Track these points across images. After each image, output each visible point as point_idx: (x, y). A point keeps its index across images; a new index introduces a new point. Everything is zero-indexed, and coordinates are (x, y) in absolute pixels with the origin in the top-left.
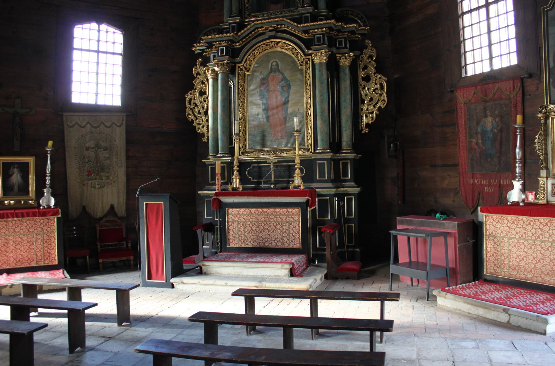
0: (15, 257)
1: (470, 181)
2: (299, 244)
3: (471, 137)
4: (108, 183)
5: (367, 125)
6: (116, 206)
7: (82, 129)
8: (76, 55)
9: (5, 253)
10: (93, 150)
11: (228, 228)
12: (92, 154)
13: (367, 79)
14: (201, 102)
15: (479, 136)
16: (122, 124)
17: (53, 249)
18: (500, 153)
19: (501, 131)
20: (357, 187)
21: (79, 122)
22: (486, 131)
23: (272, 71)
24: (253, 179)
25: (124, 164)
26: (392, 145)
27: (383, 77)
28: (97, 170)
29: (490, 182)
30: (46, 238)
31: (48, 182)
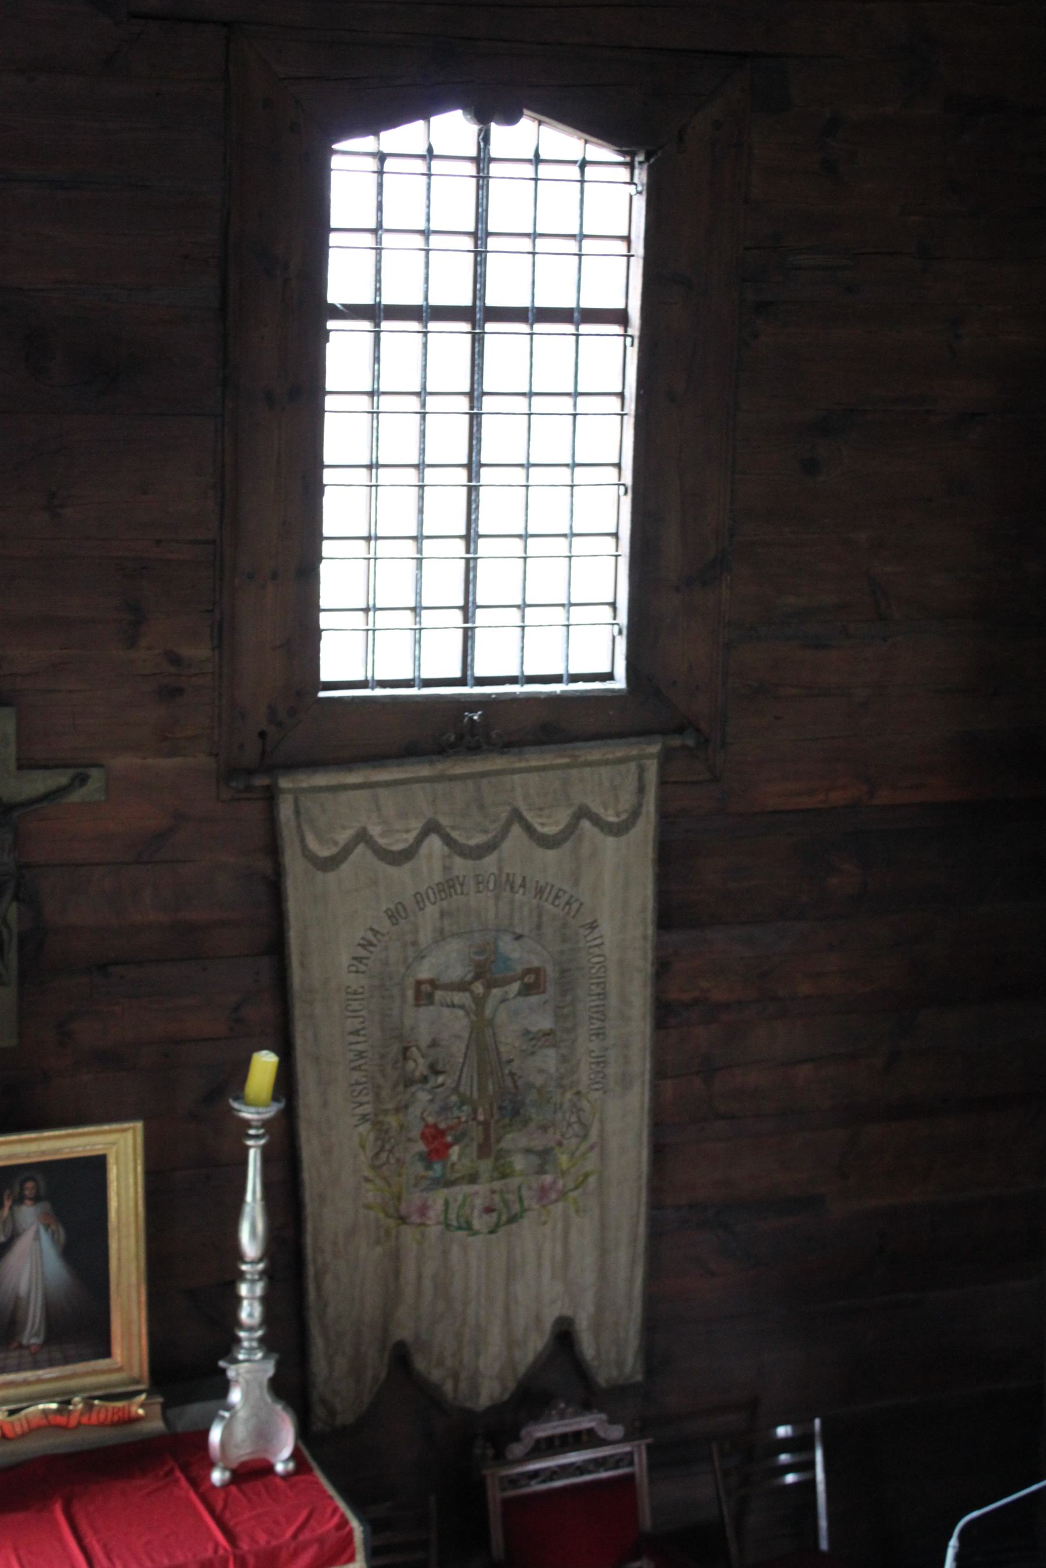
7: (392, 870)
10: (458, 997)
12: (446, 1024)
16: (635, 814)
25: (641, 1065)
28: (482, 1119)
31: (250, 1312)
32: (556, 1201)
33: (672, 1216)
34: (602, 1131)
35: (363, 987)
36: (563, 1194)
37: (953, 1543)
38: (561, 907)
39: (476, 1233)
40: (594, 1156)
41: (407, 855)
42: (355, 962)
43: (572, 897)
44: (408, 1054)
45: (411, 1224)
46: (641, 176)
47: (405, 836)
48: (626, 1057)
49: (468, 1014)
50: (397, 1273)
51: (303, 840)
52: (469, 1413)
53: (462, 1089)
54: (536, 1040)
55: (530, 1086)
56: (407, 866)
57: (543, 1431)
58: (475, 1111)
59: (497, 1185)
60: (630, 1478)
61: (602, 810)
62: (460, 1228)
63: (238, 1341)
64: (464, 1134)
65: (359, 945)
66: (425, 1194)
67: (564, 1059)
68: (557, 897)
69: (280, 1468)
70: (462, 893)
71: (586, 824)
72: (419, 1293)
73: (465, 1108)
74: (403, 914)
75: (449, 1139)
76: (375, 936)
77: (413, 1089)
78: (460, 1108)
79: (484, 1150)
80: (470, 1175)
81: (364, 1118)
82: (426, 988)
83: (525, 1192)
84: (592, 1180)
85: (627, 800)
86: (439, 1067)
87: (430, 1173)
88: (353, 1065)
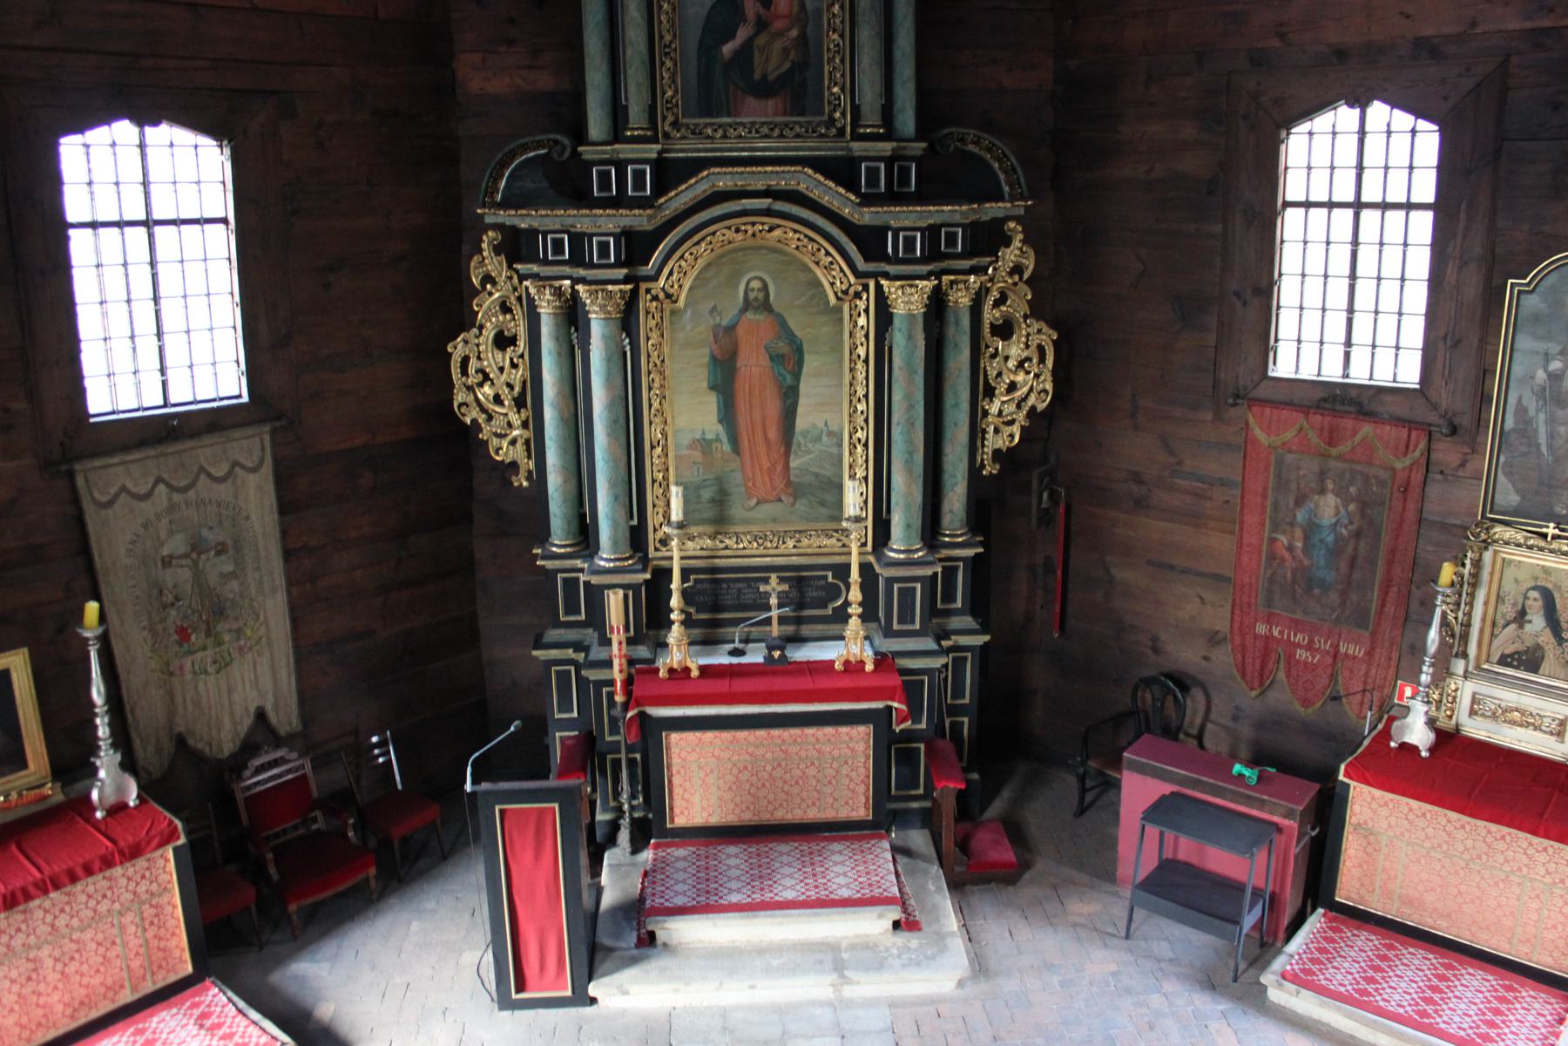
0: (67, 998)
1: (1261, 629)
2: (866, 808)
3: (1276, 527)
5: (997, 454)
6: (269, 708)
7: (143, 505)
8: (80, 245)
9: (35, 999)
10: (184, 562)
11: (670, 781)
12: (181, 576)
13: (1004, 330)
14: (502, 369)
15: (1298, 533)
16: (262, 461)
17: (173, 934)
18: (1349, 584)
19: (1358, 534)
20: (983, 632)
21: (130, 485)
22: (1318, 526)
23: (747, 305)
24: (698, 611)
25: (280, 581)
26: (1045, 495)
27: (1045, 329)
28: (206, 618)
29: (1311, 641)
30: (149, 912)
31: (103, 731)
33: (305, 650)
36: (251, 648)
37: (469, 769)
46: (227, 151)
50: (172, 699)
52: (220, 761)
57: (257, 762)
60: (304, 775)
63: (99, 747)
69: (132, 804)
71: (238, 470)
72: (185, 708)
79: (208, 633)
85: (256, 455)
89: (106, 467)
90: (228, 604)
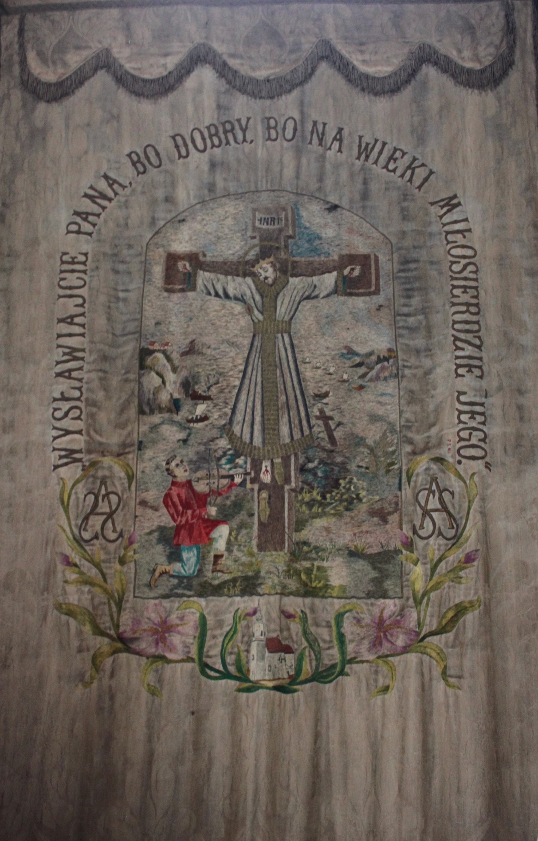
4: (382, 629)
7: (146, 107)
10: (235, 285)
12: (218, 323)
21: (122, 54)
32: (406, 650)
34: (485, 535)
35: (86, 255)
38: (399, 172)
39: (254, 687)
40: (471, 574)
41: (164, 87)
42: (78, 220)
43: (415, 159)
44: (149, 361)
45: (139, 653)
47: (162, 61)
48: (520, 408)
49: (249, 310)
51: (23, 62)
53: (237, 429)
54: (365, 366)
55: (358, 441)
56: (164, 103)
58: (256, 466)
59: (294, 604)
61: (455, 53)
62: (226, 675)
64: (238, 506)
65: (86, 195)
66: (166, 603)
67: (413, 398)
68: (391, 158)
70: (244, 140)
71: (430, 72)
73: (240, 461)
74: (154, 160)
75: (213, 511)
76: (111, 186)
77: (156, 419)
78: (231, 461)
80: (246, 578)
81: (70, 456)
82: (183, 266)
83: (348, 627)
84: (470, 618)
86: (200, 389)
87: (177, 567)
88: (59, 368)
89: (328, 754)
90: (361, 459)
